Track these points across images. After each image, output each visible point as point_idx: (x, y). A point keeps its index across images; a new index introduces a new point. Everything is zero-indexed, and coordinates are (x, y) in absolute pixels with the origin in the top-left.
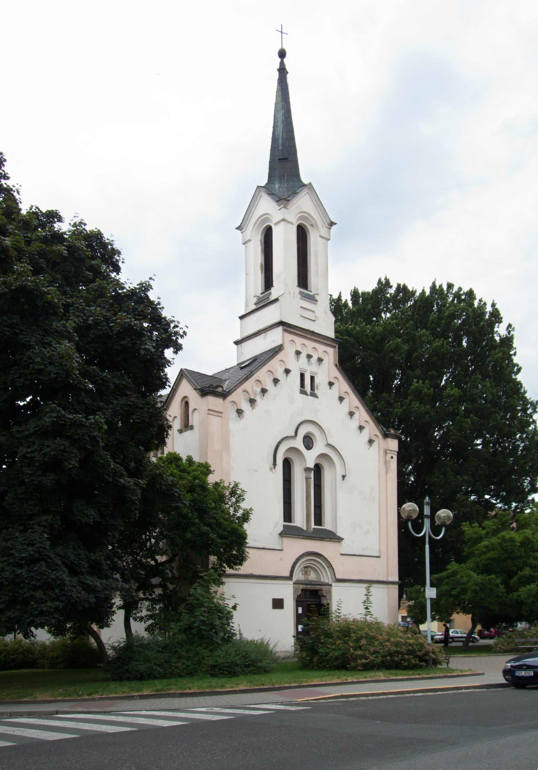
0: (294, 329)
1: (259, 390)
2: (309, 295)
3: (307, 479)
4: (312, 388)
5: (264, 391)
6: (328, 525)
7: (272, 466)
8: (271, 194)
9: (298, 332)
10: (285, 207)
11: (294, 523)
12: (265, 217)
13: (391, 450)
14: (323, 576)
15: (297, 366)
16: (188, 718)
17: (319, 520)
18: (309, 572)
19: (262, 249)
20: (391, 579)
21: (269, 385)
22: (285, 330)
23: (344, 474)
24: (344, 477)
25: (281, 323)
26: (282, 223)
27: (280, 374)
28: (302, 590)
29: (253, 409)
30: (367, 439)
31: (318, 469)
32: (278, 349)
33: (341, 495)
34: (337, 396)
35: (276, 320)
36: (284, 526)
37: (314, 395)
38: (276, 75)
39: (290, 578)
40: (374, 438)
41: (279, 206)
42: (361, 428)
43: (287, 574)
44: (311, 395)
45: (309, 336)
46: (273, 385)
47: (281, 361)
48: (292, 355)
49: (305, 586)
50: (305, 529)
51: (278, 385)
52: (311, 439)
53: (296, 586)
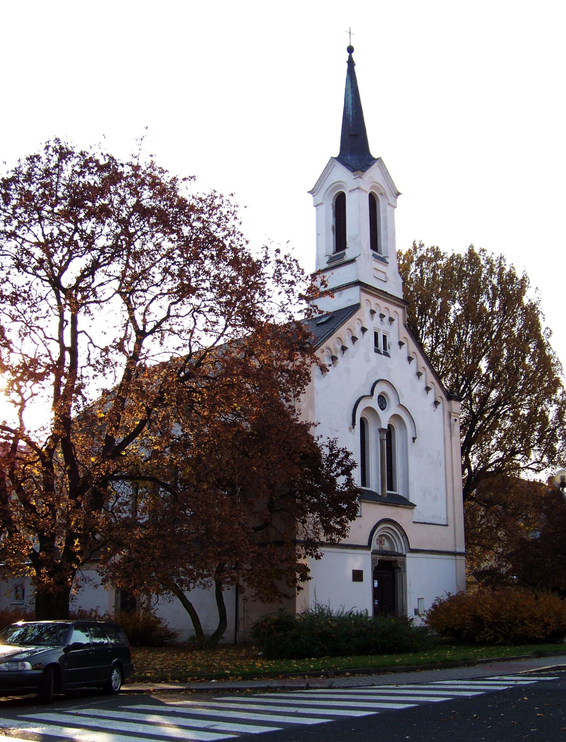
0: (370, 289)
1: (339, 347)
2: (380, 257)
3: (381, 441)
4: (385, 348)
5: (344, 349)
7: (352, 426)
8: (346, 165)
9: (373, 292)
10: (360, 177)
12: (339, 184)
13: (454, 413)
14: (397, 546)
15: (372, 324)
19: (333, 212)
20: (458, 550)
21: (348, 343)
24: (414, 439)
25: (358, 283)
26: (357, 191)
30: (433, 401)
33: (412, 459)
34: (406, 356)
35: (352, 279)
38: (346, 66)
39: (368, 547)
40: (439, 400)
41: (354, 175)
42: (427, 389)
43: (366, 543)
44: (384, 355)
45: (382, 296)
47: (359, 319)
48: (367, 314)
50: (380, 494)
53: (374, 556)
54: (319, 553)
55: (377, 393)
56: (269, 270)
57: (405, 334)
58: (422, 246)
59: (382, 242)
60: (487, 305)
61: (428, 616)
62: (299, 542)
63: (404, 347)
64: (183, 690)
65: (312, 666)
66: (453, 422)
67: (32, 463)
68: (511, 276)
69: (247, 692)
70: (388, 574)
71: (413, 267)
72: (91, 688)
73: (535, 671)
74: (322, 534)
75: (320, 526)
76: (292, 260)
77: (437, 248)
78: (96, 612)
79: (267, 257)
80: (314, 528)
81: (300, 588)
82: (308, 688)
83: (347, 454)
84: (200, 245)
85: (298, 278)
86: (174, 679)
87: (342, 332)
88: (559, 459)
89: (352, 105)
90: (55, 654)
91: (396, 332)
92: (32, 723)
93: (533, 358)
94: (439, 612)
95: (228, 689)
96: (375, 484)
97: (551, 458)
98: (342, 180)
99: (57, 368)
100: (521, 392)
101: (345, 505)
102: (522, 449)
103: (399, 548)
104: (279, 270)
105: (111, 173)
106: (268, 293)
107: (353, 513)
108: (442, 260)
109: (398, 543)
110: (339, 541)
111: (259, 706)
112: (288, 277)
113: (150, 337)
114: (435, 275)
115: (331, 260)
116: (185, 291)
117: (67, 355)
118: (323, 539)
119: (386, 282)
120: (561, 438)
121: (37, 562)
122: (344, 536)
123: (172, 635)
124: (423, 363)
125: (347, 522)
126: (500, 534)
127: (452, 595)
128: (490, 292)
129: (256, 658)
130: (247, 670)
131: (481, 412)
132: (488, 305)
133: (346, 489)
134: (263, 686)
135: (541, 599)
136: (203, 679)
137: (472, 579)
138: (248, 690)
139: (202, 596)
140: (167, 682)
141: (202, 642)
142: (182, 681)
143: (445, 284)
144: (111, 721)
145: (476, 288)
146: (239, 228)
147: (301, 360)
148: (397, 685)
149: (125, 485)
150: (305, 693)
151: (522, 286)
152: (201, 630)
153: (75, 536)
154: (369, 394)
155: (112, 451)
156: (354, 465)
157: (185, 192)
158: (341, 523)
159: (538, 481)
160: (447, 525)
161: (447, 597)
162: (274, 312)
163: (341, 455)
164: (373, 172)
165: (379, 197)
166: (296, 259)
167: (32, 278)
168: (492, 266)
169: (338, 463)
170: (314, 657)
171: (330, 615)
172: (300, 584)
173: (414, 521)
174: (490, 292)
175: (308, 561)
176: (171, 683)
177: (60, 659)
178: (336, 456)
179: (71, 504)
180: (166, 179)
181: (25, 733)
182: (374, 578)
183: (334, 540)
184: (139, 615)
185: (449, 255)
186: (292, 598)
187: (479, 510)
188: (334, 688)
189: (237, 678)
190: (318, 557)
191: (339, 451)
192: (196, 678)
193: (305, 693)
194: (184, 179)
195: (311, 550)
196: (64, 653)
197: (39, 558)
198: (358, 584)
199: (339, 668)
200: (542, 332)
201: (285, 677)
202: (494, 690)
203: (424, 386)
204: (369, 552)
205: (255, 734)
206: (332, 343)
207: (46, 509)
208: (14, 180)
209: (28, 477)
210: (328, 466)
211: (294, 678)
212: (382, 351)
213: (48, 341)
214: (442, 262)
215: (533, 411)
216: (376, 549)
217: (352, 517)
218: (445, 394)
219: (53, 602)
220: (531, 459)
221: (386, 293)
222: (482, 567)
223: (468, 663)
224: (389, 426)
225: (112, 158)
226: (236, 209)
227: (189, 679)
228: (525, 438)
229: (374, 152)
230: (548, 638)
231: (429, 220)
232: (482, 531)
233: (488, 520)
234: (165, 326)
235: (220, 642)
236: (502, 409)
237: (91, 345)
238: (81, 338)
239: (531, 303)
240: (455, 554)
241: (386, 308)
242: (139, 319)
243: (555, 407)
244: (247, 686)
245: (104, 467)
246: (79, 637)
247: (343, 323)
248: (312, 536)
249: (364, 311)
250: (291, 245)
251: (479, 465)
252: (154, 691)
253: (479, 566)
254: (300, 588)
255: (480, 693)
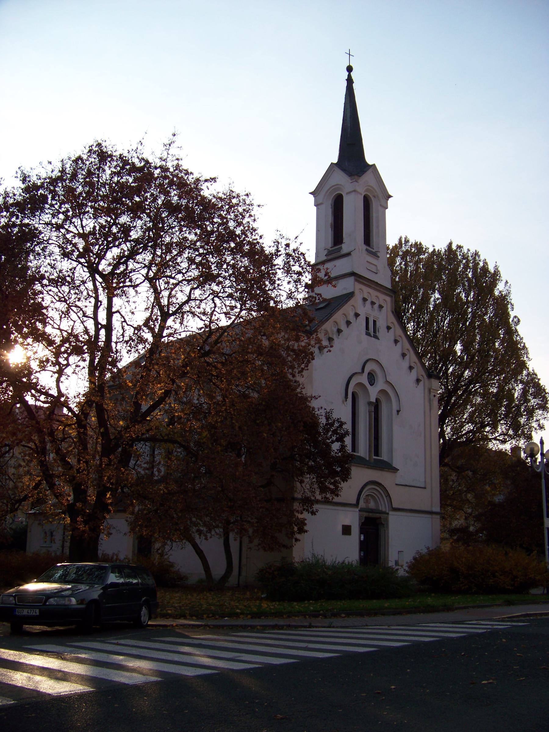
1: (335, 330)
3: (370, 412)
4: (375, 331)
5: (339, 331)
6: (384, 457)
7: (344, 399)
11: (358, 453)
12: (337, 187)
14: (381, 505)
15: (364, 310)
16: (298, 656)
17: (377, 452)
21: (343, 327)
22: (356, 280)
23: (398, 409)
24: (398, 412)
25: (353, 274)
32: (350, 296)
33: (395, 428)
34: (392, 339)
37: (376, 337)
40: (421, 378)
41: (351, 180)
42: (411, 368)
43: (354, 502)
45: (373, 286)
46: (346, 326)
47: (353, 306)
48: (360, 301)
49: (367, 514)
50: (368, 459)
51: (350, 327)
53: (361, 513)
54: (314, 509)
55: (367, 370)
56: (279, 261)
57: (392, 319)
58: (407, 241)
59: (374, 239)
60: (463, 296)
61: (409, 567)
62: (297, 499)
63: (392, 331)
64: (201, 626)
65: (312, 608)
66: (432, 397)
67: (70, 425)
68: (485, 269)
69: (258, 629)
70: (373, 529)
71: (398, 260)
72: (123, 622)
73: (522, 616)
74: (318, 492)
75: (316, 486)
76: (300, 253)
77: (420, 244)
78: (117, 556)
79: (278, 251)
80: (311, 488)
81: (297, 540)
82: (310, 626)
83: (342, 424)
84: (221, 239)
85: (305, 270)
86: (192, 616)
87: (338, 316)
88: (523, 432)
89: (350, 118)
90: (96, 593)
91: (384, 318)
92: (81, 650)
93: (502, 344)
94: (418, 563)
95: (241, 626)
96: (363, 450)
97: (516, 430)
98: (339, 183)
99: (92, 343)
100: (490, 372)
101: (336, 469)
102: (491, 422)
104: (288, 262)
105: (144, 174)
106: (277, 282)
107: (345, 475)
108: (424, 255)
109: (382, 503)
110: (332, 499)
111: (273, 641)
112: (296, 268)
113: (172, 318)
114: (418, 268)
115: (329, 253)
116: (206, 278)
117: (103, 332)
118: (319, 497)
119: (376, 273)
120: (525, 413)
121: (71, 510)
122: (337, 495)
123: (182, 578)
124: (407, 345)
125: (340, 483)
126: (469, 496)
127: (431, 549)
128: (466, 284)
129: (261, 599)
130: (255, 609)
131: (456, 388)
132: (464, 295)
133: (340, 454)
134: (271, 623)
135: (511, 554)
136: (217, 617)
137: (446, 535)
138: (259, 627)
139: (213, 546)
140: (185, 618)
141: (210, 585)
142: (199, 617)
143: (426, 276)
144: (148, 651)
145: (454, 281)
146: (255, 225)
147: (307, 341)
148: (389, 626)
149: (146, 445)
150: (310, 631)
151: (494, 280)
152: (211, 574)
153: (108, 489)
154: (360, 371)
155: (137, 417)
156: (347, 433)
157: (208, 191)
158: (335, 483)
160: (425, 488)
161: (426, 551)
162: (283, 299)
163: (336, 425)
164: (368, 176)
166: (304, 252)
167: (75, 264)
168: (468, 261)
169: (333, 431)
170: (313, 600)
171: (325, 564)
172: (298, 536)
173: (398, 483)
174: (466, 284)
175: (305, 515)
176: (193, 620)
177: (99, 596)
178: (332, 425)
179: (104, 462)
180: (191, 179)
181: (78, 658)
182: (361, 532)
183: (327, 498)
184: (155, 559)
185: (431, 250)
186: (289, 548)
187: (451, 475)
188: (333, 627)
189: (247, 616)
190: (313, 513)
191: (334, 421)
192: (211, 615)
193: (310, 631)
194: (206, 181)
195: (307, 507)
196: (102, 591)
197: (76, 508)
198: (347, 537)
199: (335, 610)
200: (511, 320)
201: (289, 617)
202: (474, 632)
203: (408, 365)
204: (357, 510)
205: (276, 665)
206: (329, 326)
207: (84, 466)
208: (60, 179)
209: (68, 438)
210: (324, 434)
211: (297, 618)
212: (372, 334)
213: (85, 319)
214: (424, 257)
215: (501, 388)
216: (362, 507)
217: (345, 479)
218: (425, 373)
219: (83, 547)
220: (498, 432)
221: (377, 283)
222: (454, 525)
223: (448, 609)
224: (377, 399)
225: (147, 162)
226: (250, 208)
227: (205, 616)
228: (493, 414)
229: (370, 159)
230: (518, 588)
231: (414, 221)
232: (453, 493)
233: (459, 484)
234: (186, 308)
235: (226, 585)
236: (474, 387)
237: (124, 324)
238: (116, 318)
239: (502, 295)
240: (431, 513)
241: (376, 296)
242: (164, 302)
243: (520, 386)
244: (257, 624)
245: (135, 431)
246: (113, 578)
247: (339, 309)
248: (309, 494)
249: (358, 297)
250: (299, 240)
251: (453, 435)
252: (177, 626)
253: (451, 524)
254: (297, 540)
255: (483, 631)
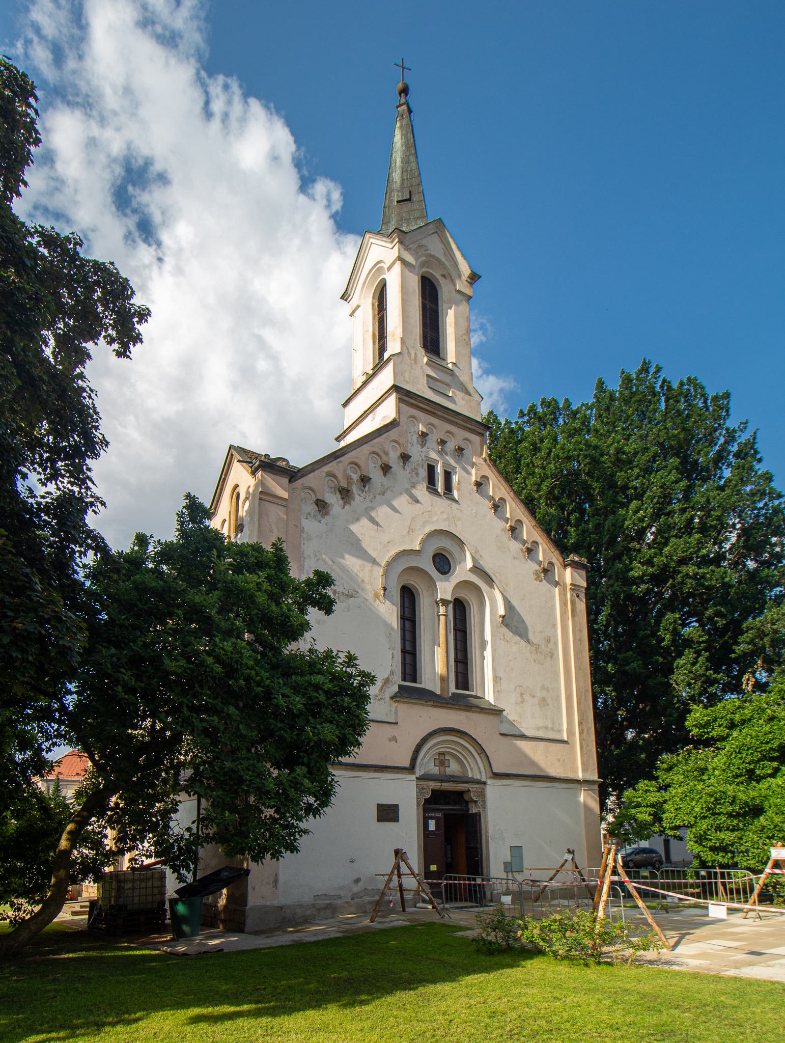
1: (355, 477)
14: (471, 769)
18: (447, 762)
21: (376, 475)
27: (393, 458)
28: (433, 791)
29: (345, 503)
31: (460, 608)
36: (400, 686)
39: (411, 768)
43: (407, 764)
45: (440, 413)
46: (382, 473)
52: (449, 564)
103: (477, 772)
159: (137, 301)
165: (441, 280)
204: (413, 777)
